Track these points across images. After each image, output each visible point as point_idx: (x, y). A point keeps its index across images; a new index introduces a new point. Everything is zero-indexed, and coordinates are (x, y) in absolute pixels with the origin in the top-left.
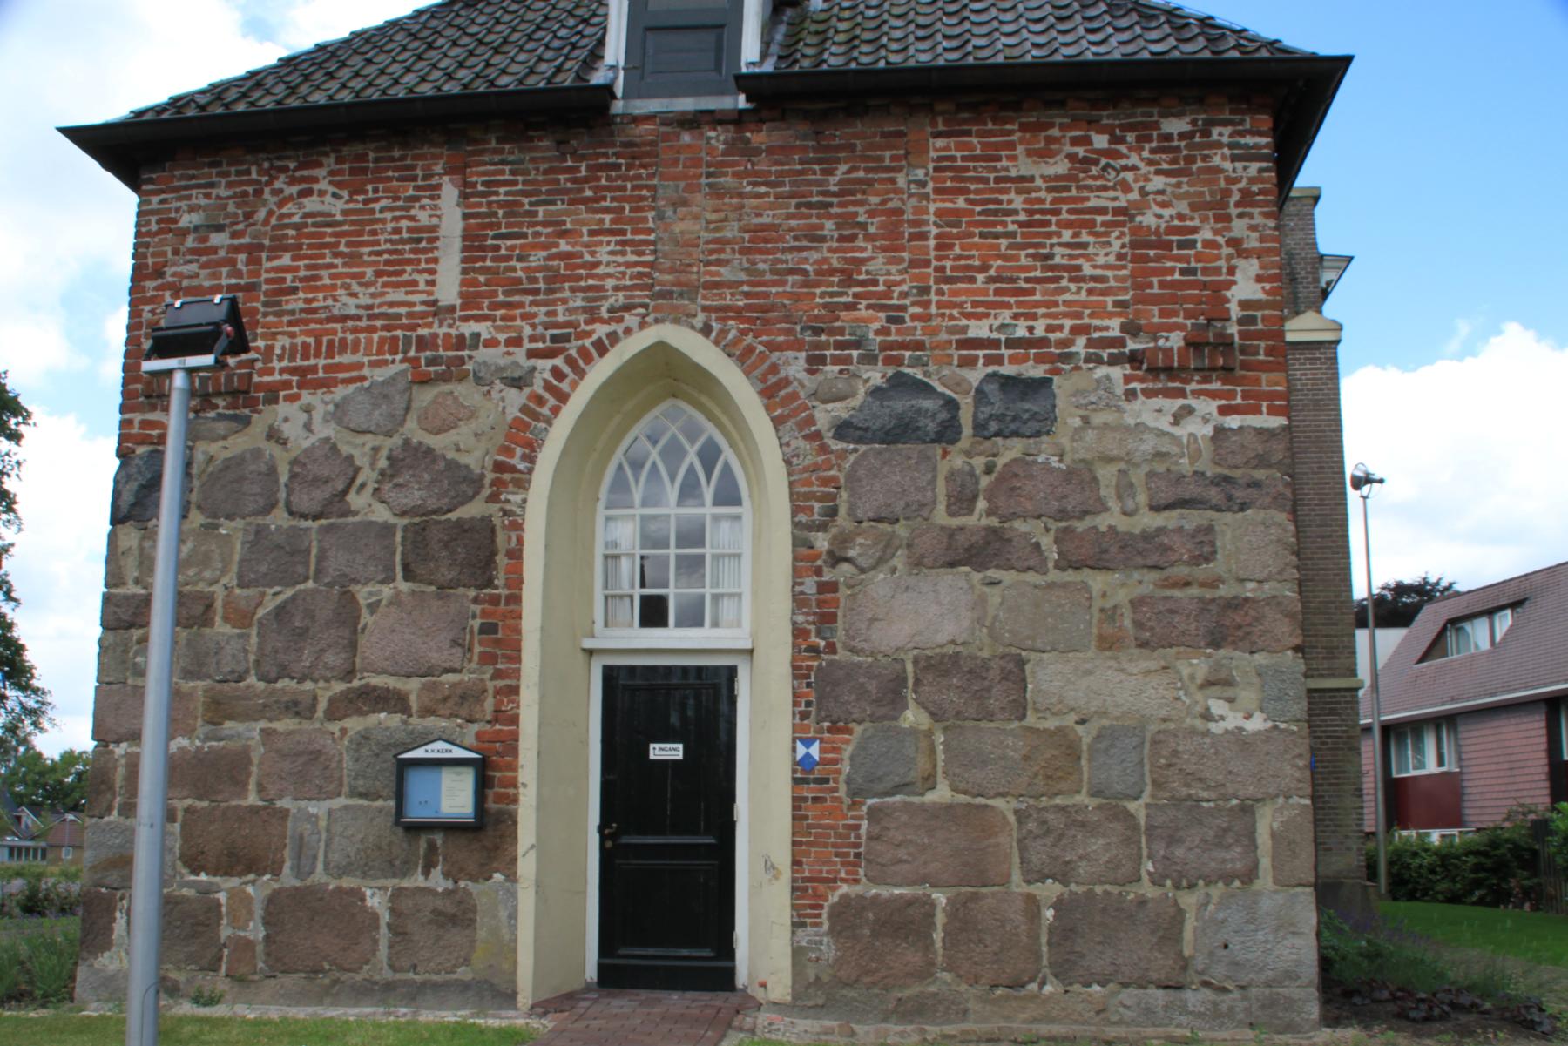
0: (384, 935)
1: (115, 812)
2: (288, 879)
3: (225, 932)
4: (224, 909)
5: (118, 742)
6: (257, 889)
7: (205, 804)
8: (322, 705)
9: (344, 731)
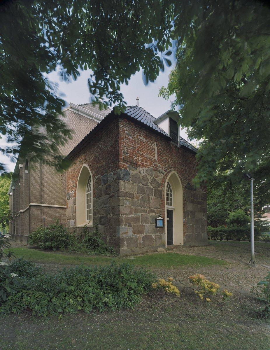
0: (154, 241)
1: (124, 225)
2: (145, 234)
3: (138, 242)
4: (142, 239)
5: (123, 215)
6: (142, 236)
7: (135, 224)
8: (147, 211)
9: (150, 215)
